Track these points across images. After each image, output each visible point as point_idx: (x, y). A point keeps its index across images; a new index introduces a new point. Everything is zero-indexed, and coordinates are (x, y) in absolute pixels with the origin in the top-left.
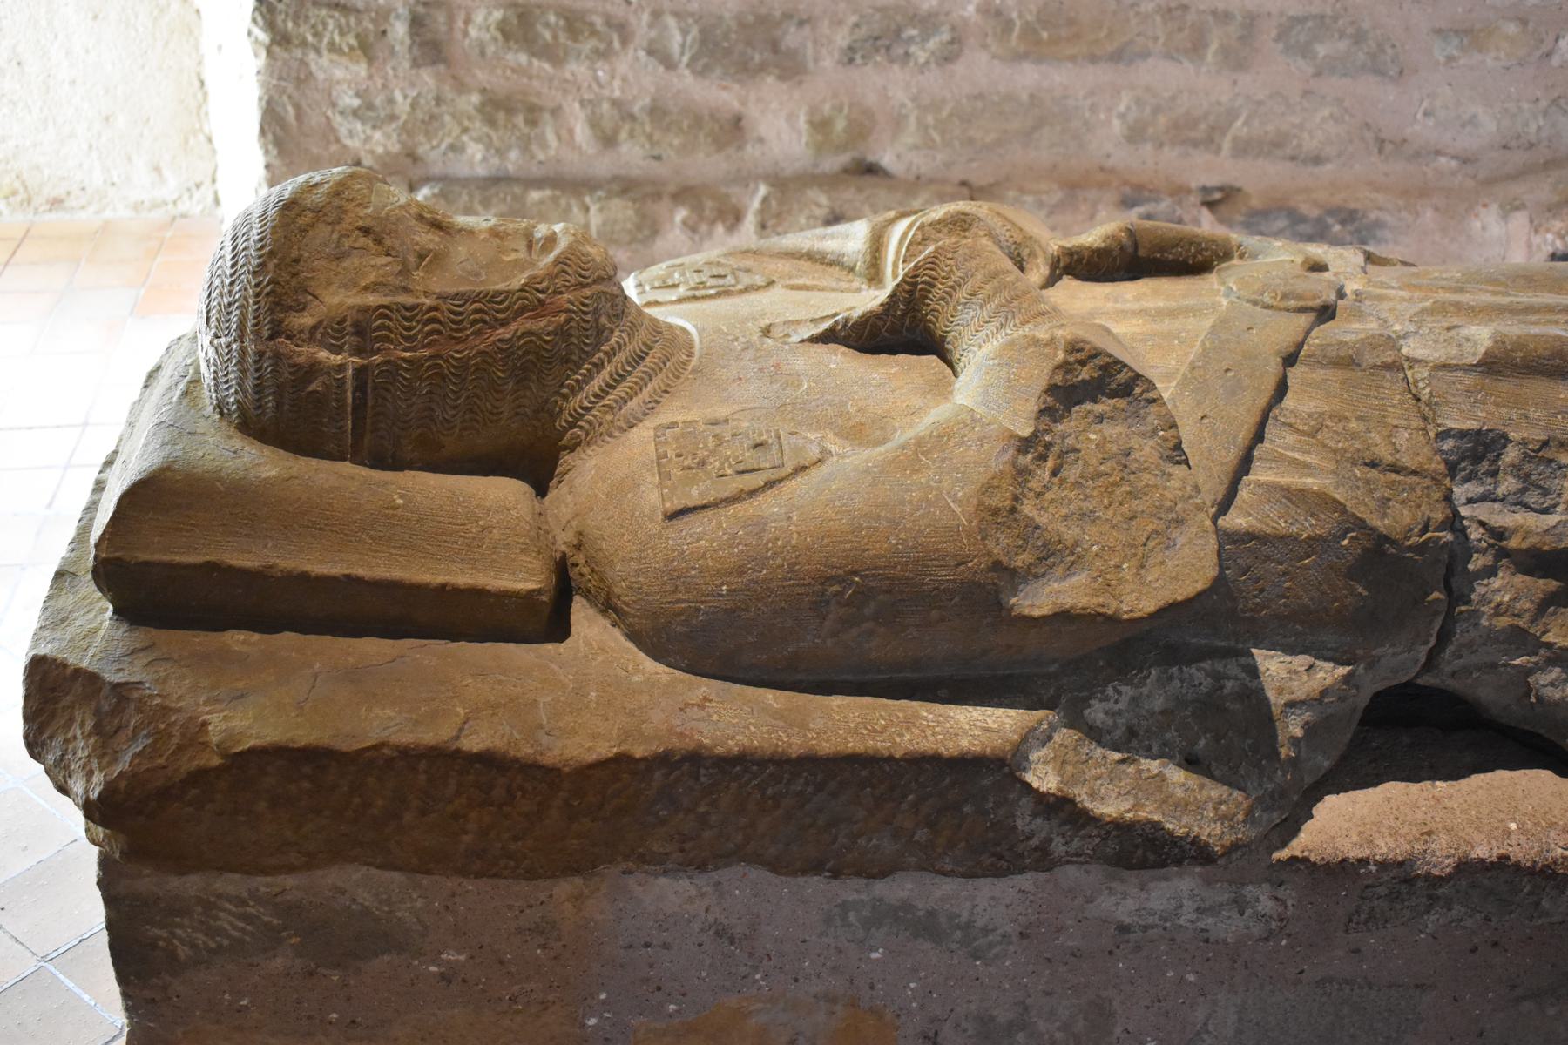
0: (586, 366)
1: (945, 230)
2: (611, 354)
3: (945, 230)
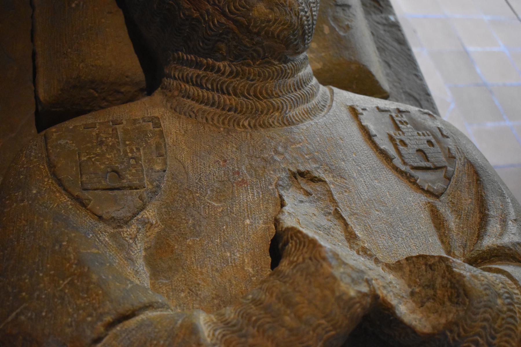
0: (192, 56)
1: (445, 282)
2: (210, 68)
3: (445, 282)
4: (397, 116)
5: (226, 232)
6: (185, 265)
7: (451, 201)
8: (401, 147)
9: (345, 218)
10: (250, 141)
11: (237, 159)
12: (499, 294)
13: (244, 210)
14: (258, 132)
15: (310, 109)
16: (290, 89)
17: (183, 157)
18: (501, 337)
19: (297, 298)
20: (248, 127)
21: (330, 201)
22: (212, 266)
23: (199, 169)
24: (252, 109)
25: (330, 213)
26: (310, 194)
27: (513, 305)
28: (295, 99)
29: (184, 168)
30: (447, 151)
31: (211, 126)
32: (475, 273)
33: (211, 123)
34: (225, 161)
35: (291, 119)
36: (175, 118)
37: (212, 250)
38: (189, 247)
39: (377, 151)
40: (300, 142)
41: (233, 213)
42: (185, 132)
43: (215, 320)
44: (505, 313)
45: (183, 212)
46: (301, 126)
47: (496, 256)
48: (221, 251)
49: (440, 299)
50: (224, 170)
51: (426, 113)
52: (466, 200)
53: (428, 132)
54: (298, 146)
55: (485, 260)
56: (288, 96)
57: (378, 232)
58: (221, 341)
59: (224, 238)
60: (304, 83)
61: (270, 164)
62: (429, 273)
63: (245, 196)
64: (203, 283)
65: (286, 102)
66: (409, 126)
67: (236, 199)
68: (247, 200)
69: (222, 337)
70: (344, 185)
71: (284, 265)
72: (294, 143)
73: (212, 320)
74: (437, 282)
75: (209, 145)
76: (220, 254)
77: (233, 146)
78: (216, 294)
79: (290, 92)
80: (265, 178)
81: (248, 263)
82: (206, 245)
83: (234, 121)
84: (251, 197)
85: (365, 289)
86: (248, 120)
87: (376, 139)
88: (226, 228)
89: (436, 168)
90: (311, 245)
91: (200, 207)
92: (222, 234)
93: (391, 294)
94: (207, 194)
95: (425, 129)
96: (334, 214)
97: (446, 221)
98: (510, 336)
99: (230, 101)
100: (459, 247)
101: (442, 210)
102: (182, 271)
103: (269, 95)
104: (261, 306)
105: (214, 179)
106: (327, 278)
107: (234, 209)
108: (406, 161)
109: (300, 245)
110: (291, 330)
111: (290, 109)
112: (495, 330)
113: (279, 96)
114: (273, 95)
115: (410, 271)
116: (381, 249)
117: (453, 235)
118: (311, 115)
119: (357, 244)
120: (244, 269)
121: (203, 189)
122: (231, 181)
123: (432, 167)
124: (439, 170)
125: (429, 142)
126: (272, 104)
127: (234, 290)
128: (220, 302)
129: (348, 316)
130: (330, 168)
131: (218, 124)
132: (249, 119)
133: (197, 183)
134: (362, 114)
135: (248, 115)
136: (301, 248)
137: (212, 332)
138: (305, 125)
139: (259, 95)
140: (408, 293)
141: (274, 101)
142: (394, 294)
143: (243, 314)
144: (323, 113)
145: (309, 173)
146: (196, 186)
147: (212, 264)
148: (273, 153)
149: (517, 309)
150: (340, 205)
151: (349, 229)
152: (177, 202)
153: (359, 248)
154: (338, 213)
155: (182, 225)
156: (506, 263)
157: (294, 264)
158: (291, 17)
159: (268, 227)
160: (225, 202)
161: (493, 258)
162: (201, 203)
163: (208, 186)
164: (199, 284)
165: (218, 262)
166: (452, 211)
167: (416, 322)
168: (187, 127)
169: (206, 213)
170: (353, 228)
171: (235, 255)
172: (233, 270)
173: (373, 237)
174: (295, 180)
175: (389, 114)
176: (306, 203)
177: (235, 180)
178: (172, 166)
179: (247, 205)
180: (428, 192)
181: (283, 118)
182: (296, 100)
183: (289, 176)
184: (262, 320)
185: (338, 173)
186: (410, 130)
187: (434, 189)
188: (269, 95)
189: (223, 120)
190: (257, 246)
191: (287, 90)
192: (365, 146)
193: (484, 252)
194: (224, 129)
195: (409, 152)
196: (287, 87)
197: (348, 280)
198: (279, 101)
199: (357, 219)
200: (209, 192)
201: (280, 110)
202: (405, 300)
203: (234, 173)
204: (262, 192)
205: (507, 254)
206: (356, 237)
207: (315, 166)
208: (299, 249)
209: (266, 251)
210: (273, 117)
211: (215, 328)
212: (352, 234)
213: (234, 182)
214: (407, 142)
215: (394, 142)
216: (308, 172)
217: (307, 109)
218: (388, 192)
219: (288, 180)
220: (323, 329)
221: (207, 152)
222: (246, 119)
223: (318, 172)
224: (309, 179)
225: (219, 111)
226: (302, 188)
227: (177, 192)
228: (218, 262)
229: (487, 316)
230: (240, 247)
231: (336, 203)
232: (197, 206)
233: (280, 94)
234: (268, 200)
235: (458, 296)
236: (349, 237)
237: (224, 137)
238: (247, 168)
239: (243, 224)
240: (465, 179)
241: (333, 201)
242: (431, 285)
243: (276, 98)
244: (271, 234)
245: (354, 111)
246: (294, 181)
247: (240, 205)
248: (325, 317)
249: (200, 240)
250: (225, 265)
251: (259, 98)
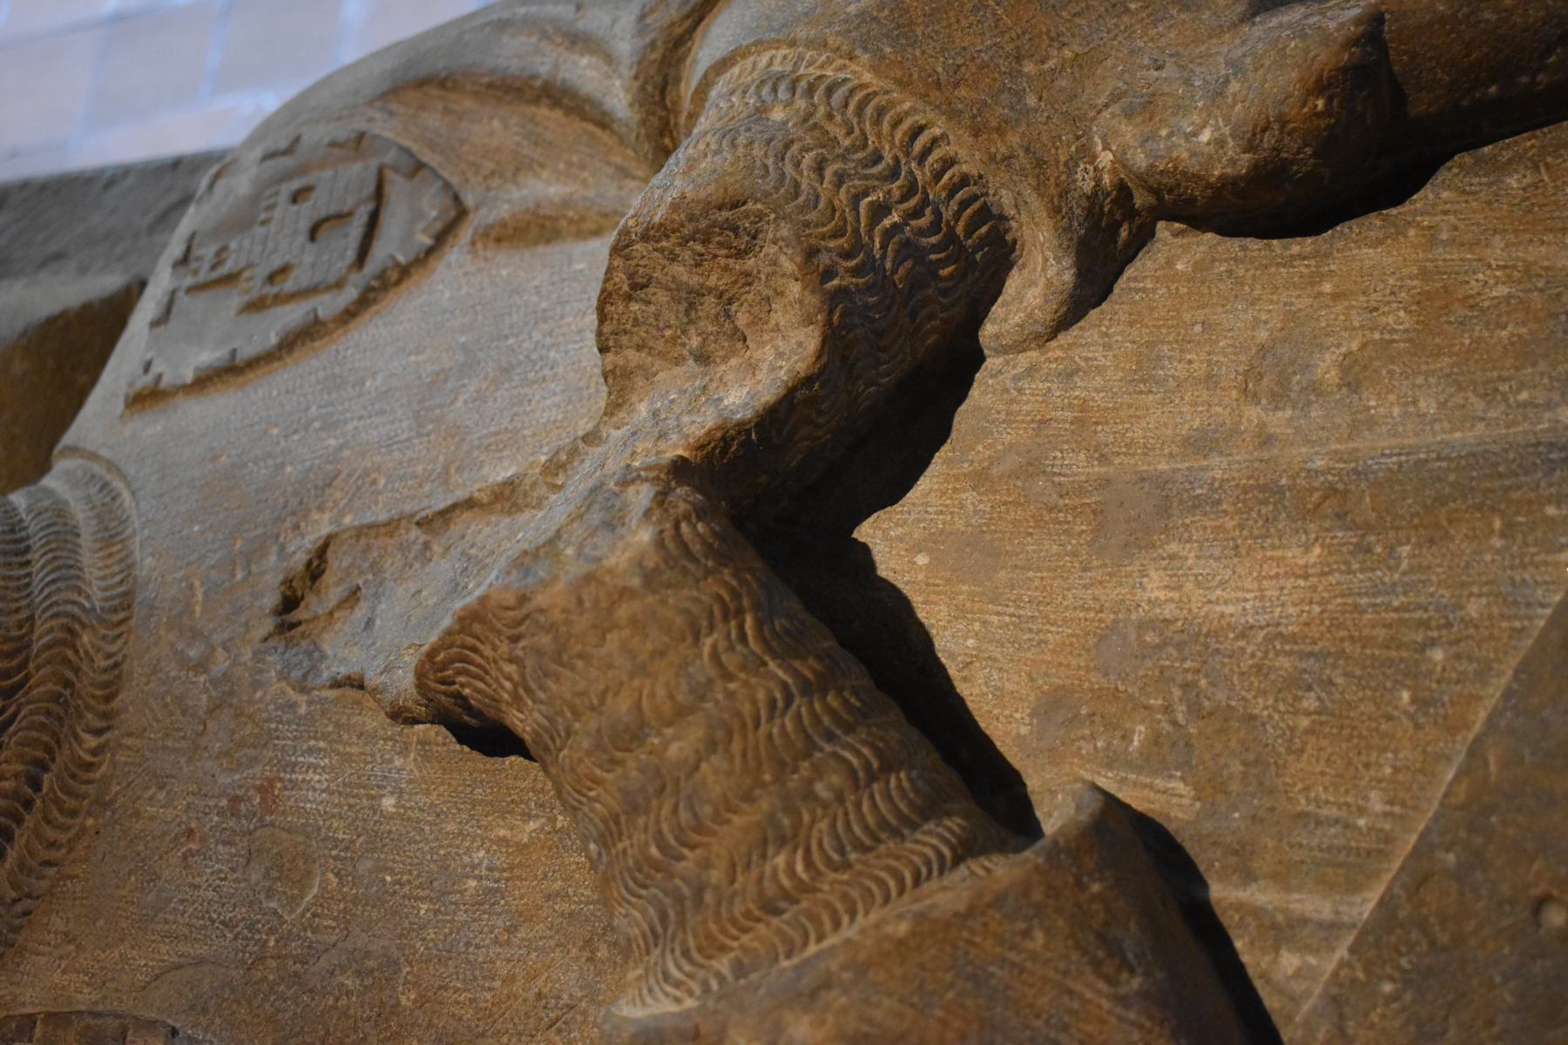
4: (196, 273)
5: (405, 878)
6: (473, 1024)
7: (485, 178)
8: (289, 285)
9: (449, 502)
10: (146, 741)
11: (193, 794)
12: (757, 110)
13: (350, 806)
14: (127, 710)
15: (98, 531)
16: (19, 579)
17: (145, 965)
18: (879, 136)
19: (622, 706)
20: (102, 739)
21: (391, 537)
22: (496, 942)
23: (194, 921)
24: (48, 713)
25: (426, 545)
26: (355, 593)
27: (798, 79)
28: (53, 571)
29: (180, 967)
30: (336, 151)
31: (73, 855)
32: (682, 163)
33: (64, 851)
34: (190, 833)
35: (113, 598)
36: (18, 965)
37: (447, 931)
38: (421, 1001)
39: (280, 358)
40: (191, 587)
41: (353, 842)
42: (69, 942)
43: (640, 971)
44: (815, 107)
45: (313, 999)
46: (144, 573)
47: (663, 91)
48: (455, 903)
49: (735, 282)
50: (217, 843)
51: (211, 186)
53: (268, 193)
54: (199, 595)
55: (667, 123)
56: (36, 593)
57: (516, 414)
58: (701, 966)
59: (420, 886)
60: (12, 531)
62: (655, 294)
63: (310, 793)
64: (540, 982)
65: (57, 603)
66: (233, 245)
67: (310, 825)
68: (323, 791)
69: (691, 960)
70: (355, 482)
71: (522, 722)
72: (188, 609)
73: (639, 978)
74: (684, 278)
75: (130, 874)
76: (465, 912)
77: (151, 799)
78: (581, 949)
79: (27, 580)
80: (269, 720)
81: (512, 829)
82: (427, 948)
83: (73, 776)
84: (317, 777)
85: (642, 496)
86: (82, 734)
87: (247, 351)
88: (392, 872)
89: (379, 195)
90: (477, 627)
91: (312, 942)
92: (406, 889)
93: (686, 419)
94: (275, 912)
95: (255, 199)
96: (432, 532)
97: (538, 206)
98: (881, 112)
99: (6, 779)
100: (620, 188)
101: (504, 211)
102: (490, 1040)
103: (18, 651)
104: (623, 819)
105: (237, 881)
106: (580, 602)
107: (340, 836)
108: (332, 279)
109: (471, 662)
110: (712, 746)
111: (80, 591)
112: (853, 149)
115: (639, 348)
116: (566, 418)
117: (585, 198)
118: (117, 534)
119: (534, 485)
120: (525, 845)
121: (258, 921)
122: (256, 828)
123: (370, 206)
124: (388, 189)
125: (296, 198)
126: (48, 647)
127: (581, 891)
128: (606, 941)
129: (710, 563)
130: (293, 513)
131: (73, 832)
132: (79, 730)
133: (236, 938)
134: (159, 377)
135: (65, 730)
136: (478, 659)
137: (668, 989)
138: (142, 560)
139: (10, 682)
140: (698, 369)
141: (40, 638)
142: (689, 412)
143: (635, 880)
144: (126, 494)
145: (291, 581)
146: (244, 942)
147: (487, 942)
148: (202, 679)
149: (811, 70)
150: (408, 507)
151: (485, 499)
152: (278, 1011)
153: (546, 483)
154: (432, 520)
155: (352, 1011)
156: (691, 66)
157: (521, 691)
159: (419, 742)
160: (314, 862)
161: (668, 102)
162: (300, 938)
163: (251, 904)
164: (539, 996)
165: (489, 920)
166: (517, 184)
167: (781, 367)
168: (56, 933)
169: (334, 928)
170: (484, 484)
171: (480, 864)
172: (520, 878)
173: (527, 432)
174: (301, 628)
175: (181, 294)
176: (378, 612)
177: (254, 814)
178: (166, 1005)
179: (340, 794)
180: (443, 237)
181: (101, 621)
182: (59, 568)
183: (283, 643)
184: (665, 827)
185: (313, 492)
186: (246, 243)
187: (435, 219)
188: (18, 651)
189: (61, 810)
190: (469, 790)
191: (18, 589)
192: (256, 392)
193: (643, 122)
194: (89, 814)
195: (311, 263)
196: (7, 588)
197: (602, 540)
198: (46, 621)
199: (459, 470)
200: (273, 905)
201: (77, 626)
202: (715, 385)
203: (232, 815)
204: (310, 738)
205: (664, 56)
206: (512, 483)
207: (273, 558)
208: (479, 666)
209: (488, 766)
210: (91, 651)
211: (660, 976)
212: (502, 493)
213: (261, 820)
214: (277, 262)
215: (269, 302)
216: (288, 582)
217: (96, 540)
218: (409, 354)
219: (294, 651)
220: (731, 648)
221: (148, 882)
222: (77, 737)
223: (294, 553)
224: (309, 583)
225: (30, 820)
226: (331, 614)
227: (250, 1005)
228: (489, 920)
229: (808, 159)
230: (458, 842)
231: (399, 520)
232: (306, 950)
233: (24, 615)
234: (337, 725)
235: (735, 229)
236: (508, 505)
237: (116, 822)
238: (226, 769)
239: (392, 818)
240: (433, 120)
241: (390, 527)
242: (690, 299)
243: (32, 631)
244: (440, 739)
245: (147, 398)
246: (303, 633)
247: (334, 816)
248: (697, 636)
249: (410, 964)
250: (502, 902)
251: (20, 685)
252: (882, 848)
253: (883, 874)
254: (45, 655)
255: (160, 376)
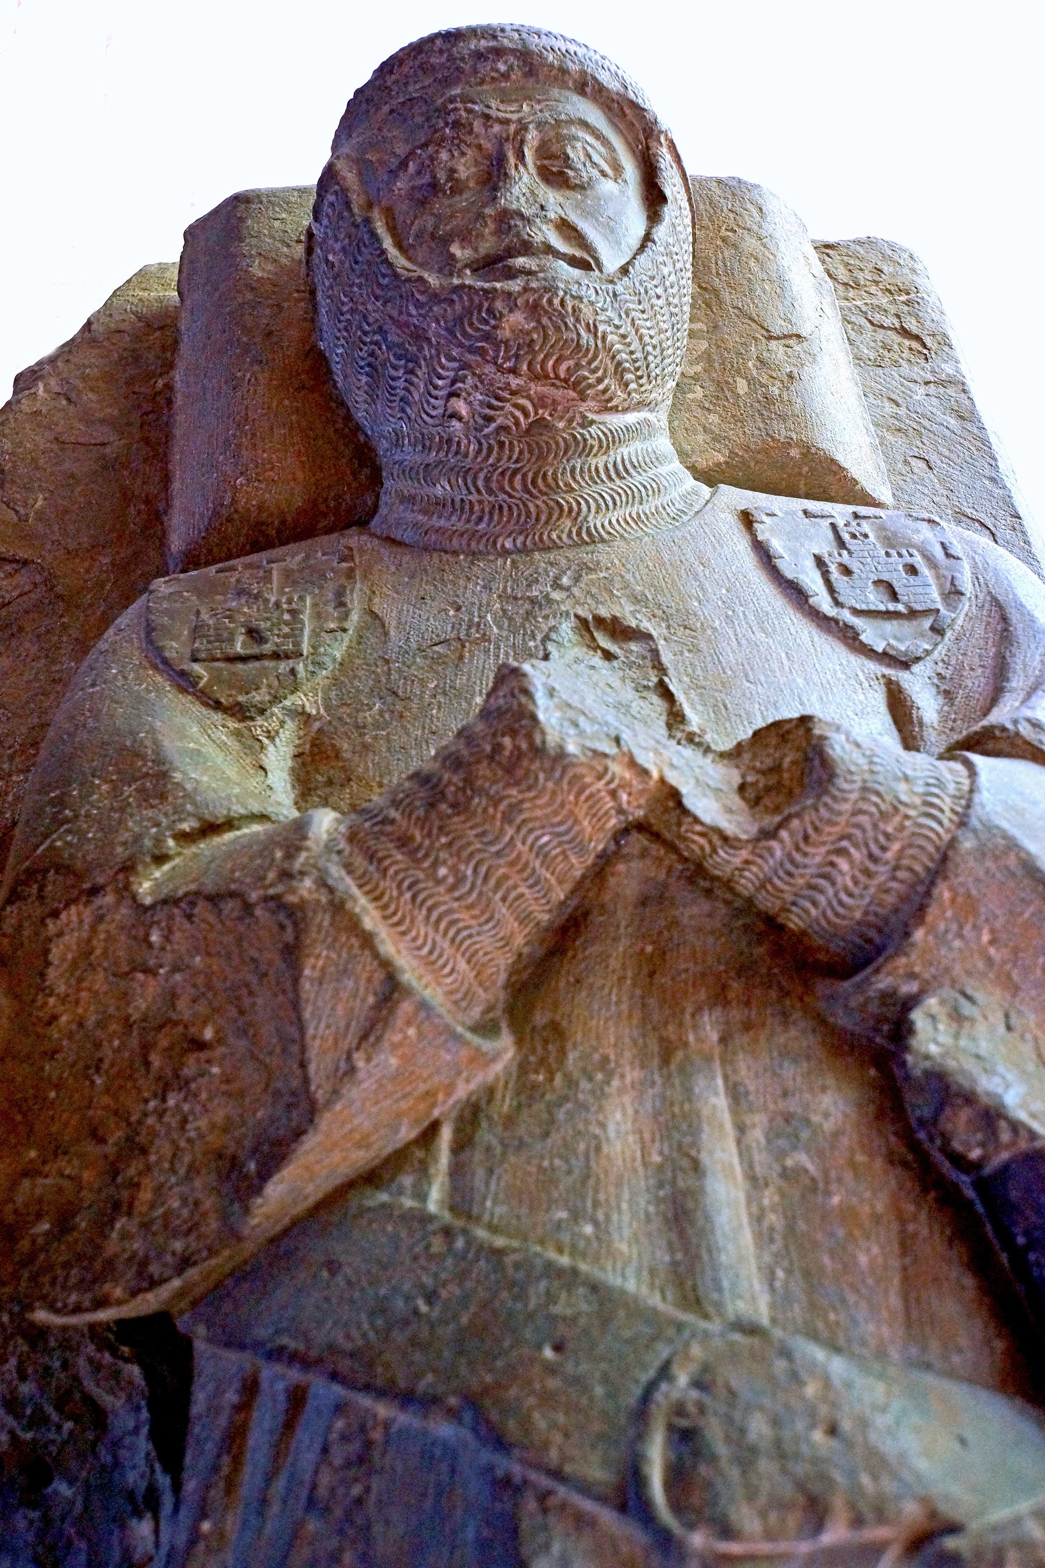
39: (780, 585)
52: (972, 669)
61: (540, 606)
87: (778, 563)
89: (913, 614)
103: (551, 488)
108: (841, 599)
113: (573, 490)
114: (558, 486)
126: (558, 502)
158: (579, 334)
175: (830, 521)
180: (887, 658)
188: (551, 488)
191: (591, 478)
226: (599, 647)
241: (660, 668)
243: (566, 492)
245: (747, 519)
252: (416, 912)
253: (400, 914)
254: (552, 503)
255: (762, 522)
